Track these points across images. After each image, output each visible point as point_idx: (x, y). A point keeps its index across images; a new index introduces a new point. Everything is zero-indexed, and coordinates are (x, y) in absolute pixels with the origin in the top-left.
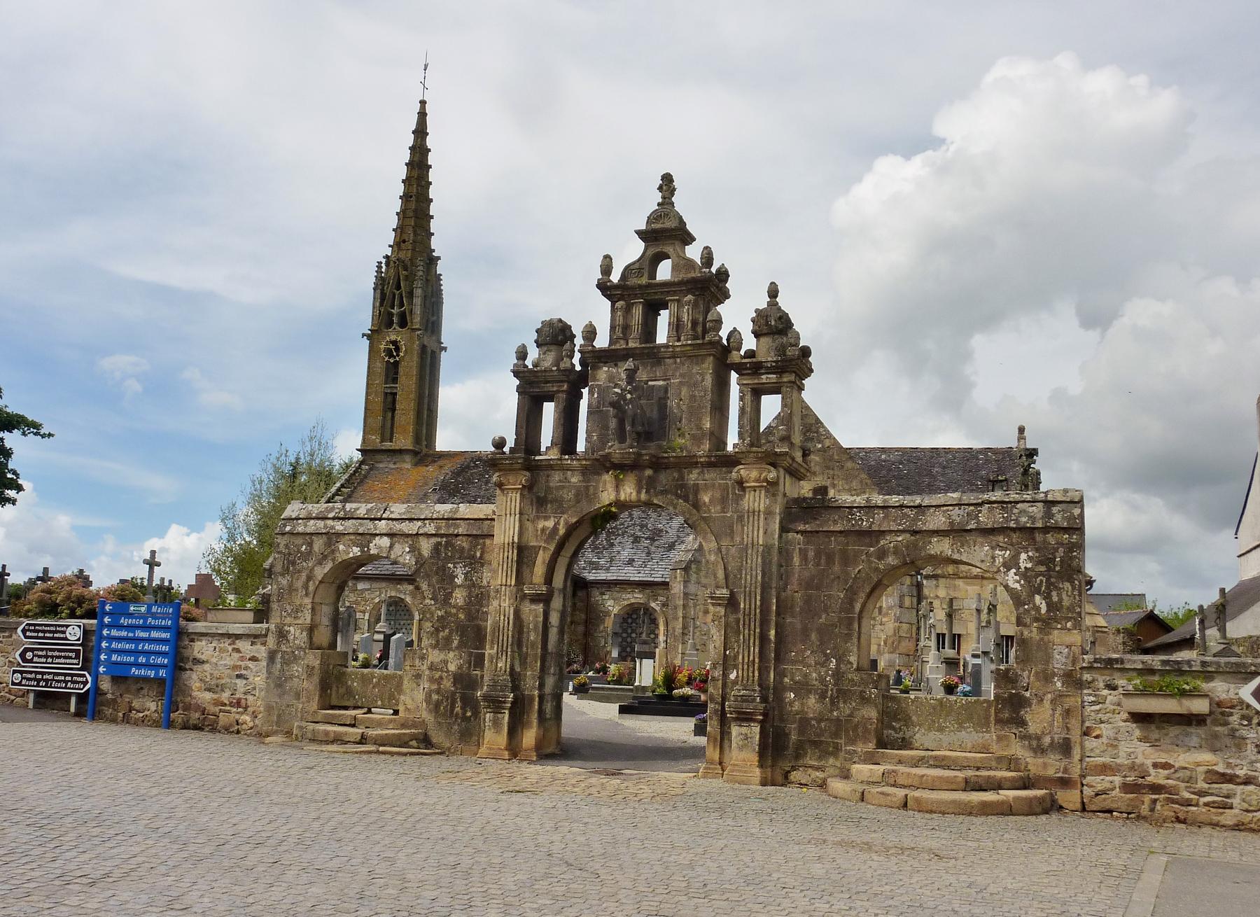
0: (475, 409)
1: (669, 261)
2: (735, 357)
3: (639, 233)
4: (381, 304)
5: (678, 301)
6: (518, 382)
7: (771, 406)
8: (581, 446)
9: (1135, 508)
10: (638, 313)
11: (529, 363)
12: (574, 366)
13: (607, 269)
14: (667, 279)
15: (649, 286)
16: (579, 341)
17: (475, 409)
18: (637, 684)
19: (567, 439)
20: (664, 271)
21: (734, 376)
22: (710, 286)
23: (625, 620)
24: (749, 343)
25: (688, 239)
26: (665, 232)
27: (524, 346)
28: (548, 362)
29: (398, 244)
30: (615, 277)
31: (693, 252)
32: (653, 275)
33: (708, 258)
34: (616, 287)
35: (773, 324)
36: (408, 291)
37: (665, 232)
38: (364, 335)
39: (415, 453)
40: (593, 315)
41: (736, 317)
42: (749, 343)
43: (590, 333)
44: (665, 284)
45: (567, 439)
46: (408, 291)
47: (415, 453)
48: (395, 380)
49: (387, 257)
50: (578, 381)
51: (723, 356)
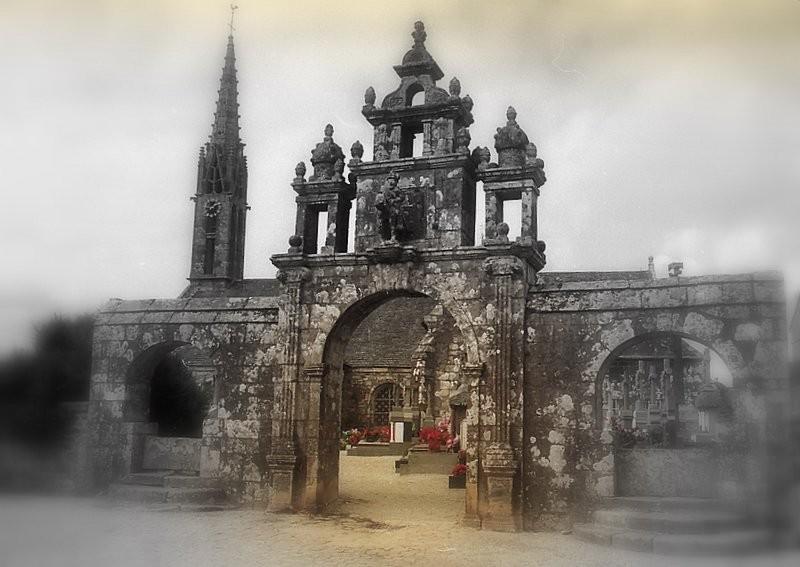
0: (269, 226)
1: (423, 93)
2: (483, 167)
3: (395, 68)
4: (204, 177)
5: (432, 123)
6: (298, 195)
7: (513, 212)
8: (351, 248)
9: (727, 426)
10: (396, 134)
11: (307, 177)
12: (344, 179)
13: (370, 96)
14: (419, 103)
15: (406, 110)
16: (348, 158)
17: (269, 226)
18: (392, 441)
19: (339, 240)
20: (419, 100)
21: (480, 185)
22: (459, 112)
23: (379, 396)
24: (494, 158)
25: (437, 73)
26: (418, 66)
27: (303, 164)
28: (322, 179)
29: (216, 134)
30: (378, 104)
31: (444, 84)
32: (409, 102)
33: (456, 87)
34: (378, 113)
35: (513, 141)
36: (222, 175)
37: (418, 66)
38: (192, 198)
39: (228, 281)
40: (356, 134)
41: (482, 135)
42: (494, 158)
43: (358, 150)
44: (418, 108)
45: (339, 240)
46: (222, 175)
47: (228, 281)
48: (214, 230)
49: (208, 144)
50: (348, 193)
51: (473, 167)
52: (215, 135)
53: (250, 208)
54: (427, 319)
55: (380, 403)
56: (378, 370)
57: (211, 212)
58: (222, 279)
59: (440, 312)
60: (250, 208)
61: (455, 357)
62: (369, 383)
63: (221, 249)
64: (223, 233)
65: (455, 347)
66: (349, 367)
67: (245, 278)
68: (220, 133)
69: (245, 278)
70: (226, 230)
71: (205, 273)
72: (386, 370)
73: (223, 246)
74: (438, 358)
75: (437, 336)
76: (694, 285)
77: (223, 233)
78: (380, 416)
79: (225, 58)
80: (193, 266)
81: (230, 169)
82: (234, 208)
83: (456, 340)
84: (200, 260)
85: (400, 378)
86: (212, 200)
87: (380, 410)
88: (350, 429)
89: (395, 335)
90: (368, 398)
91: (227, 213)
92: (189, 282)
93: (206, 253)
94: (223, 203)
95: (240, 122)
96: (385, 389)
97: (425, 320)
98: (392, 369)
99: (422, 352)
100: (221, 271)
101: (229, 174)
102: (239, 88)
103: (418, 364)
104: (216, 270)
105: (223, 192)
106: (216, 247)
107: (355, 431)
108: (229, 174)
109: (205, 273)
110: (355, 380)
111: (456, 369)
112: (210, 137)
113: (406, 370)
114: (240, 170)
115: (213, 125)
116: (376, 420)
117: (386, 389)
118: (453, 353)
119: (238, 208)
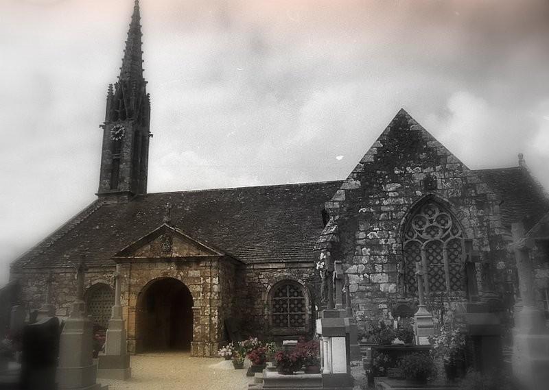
4: (111, 108)
23: (276, 295)
38: (100, 126)
39: (131, 195)
52: (121, 74)
53: (152, 135)
54: (328, 205)
55: (277, 302)
56: (275, 266)
57: (117, 136)
58: (125, 193)
59: (343, 197)
60: (152, 135)
61: (362, 246)
62: (266, 281)
63: (125, 167)
64: (127, 153)
65: (361, 235)
66: (243, 263)
67: (148, 192)
68: (126, 73)
69: (148, 192)
70: (129, 150)
71: (111, 188)
72: (283, 266)
73: (126, 164)
74: (344, 249)
75: (340, 223)
76: (444, 386)
77: (127, 153)
78: (278, 317)
79: (142, 35)
80: (100, 183)
81: (133, 98)
82: (136, 134)
83: (362, 227)
84: (106, 178)
85: (300, 274)
86: (118, 126)
87: (278, 310)
88: (247, 338)
89: (288, 231)
90: (265, 297)
91: (130, 135)
92: (97, 197)
93: (112, 172)
94: (126, 128)
95: (144, 66)
96: (286, 287)
97: (326, 207)
98: (290, 264)
99: (325, 242)
100: (124, 186)
101: (133, 103)
102: (143, 39)
103: (322, 256)
104: (121, 186)
105: (128, 119)
106: (121, 166)
107: (255, 341)
108: (133, 103)
109: (111, 188)
110: (249, 277)
111: (364, 260)
112: (118, 77)
113: (305, 265)
114: (143, 103)
115: (121, 68)
116: (274, 321)
117: (284, 287)
118: (360, 242)
119: (140, 134)
